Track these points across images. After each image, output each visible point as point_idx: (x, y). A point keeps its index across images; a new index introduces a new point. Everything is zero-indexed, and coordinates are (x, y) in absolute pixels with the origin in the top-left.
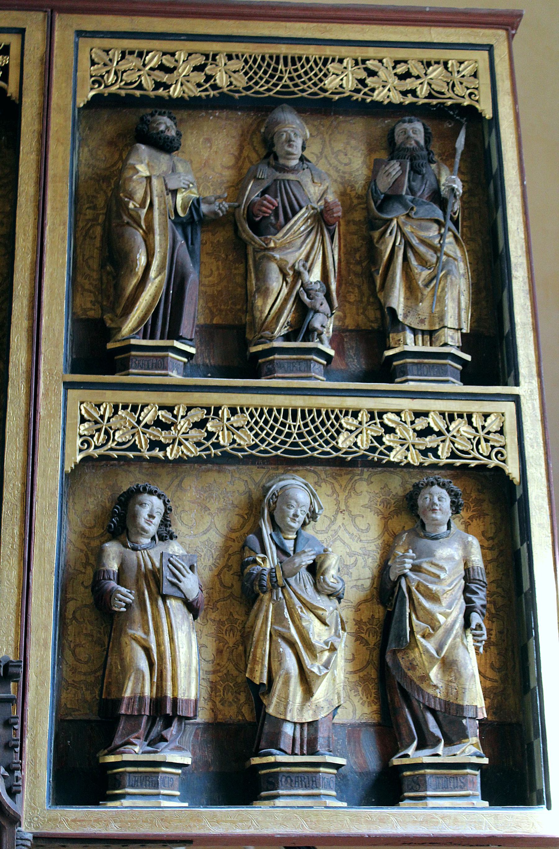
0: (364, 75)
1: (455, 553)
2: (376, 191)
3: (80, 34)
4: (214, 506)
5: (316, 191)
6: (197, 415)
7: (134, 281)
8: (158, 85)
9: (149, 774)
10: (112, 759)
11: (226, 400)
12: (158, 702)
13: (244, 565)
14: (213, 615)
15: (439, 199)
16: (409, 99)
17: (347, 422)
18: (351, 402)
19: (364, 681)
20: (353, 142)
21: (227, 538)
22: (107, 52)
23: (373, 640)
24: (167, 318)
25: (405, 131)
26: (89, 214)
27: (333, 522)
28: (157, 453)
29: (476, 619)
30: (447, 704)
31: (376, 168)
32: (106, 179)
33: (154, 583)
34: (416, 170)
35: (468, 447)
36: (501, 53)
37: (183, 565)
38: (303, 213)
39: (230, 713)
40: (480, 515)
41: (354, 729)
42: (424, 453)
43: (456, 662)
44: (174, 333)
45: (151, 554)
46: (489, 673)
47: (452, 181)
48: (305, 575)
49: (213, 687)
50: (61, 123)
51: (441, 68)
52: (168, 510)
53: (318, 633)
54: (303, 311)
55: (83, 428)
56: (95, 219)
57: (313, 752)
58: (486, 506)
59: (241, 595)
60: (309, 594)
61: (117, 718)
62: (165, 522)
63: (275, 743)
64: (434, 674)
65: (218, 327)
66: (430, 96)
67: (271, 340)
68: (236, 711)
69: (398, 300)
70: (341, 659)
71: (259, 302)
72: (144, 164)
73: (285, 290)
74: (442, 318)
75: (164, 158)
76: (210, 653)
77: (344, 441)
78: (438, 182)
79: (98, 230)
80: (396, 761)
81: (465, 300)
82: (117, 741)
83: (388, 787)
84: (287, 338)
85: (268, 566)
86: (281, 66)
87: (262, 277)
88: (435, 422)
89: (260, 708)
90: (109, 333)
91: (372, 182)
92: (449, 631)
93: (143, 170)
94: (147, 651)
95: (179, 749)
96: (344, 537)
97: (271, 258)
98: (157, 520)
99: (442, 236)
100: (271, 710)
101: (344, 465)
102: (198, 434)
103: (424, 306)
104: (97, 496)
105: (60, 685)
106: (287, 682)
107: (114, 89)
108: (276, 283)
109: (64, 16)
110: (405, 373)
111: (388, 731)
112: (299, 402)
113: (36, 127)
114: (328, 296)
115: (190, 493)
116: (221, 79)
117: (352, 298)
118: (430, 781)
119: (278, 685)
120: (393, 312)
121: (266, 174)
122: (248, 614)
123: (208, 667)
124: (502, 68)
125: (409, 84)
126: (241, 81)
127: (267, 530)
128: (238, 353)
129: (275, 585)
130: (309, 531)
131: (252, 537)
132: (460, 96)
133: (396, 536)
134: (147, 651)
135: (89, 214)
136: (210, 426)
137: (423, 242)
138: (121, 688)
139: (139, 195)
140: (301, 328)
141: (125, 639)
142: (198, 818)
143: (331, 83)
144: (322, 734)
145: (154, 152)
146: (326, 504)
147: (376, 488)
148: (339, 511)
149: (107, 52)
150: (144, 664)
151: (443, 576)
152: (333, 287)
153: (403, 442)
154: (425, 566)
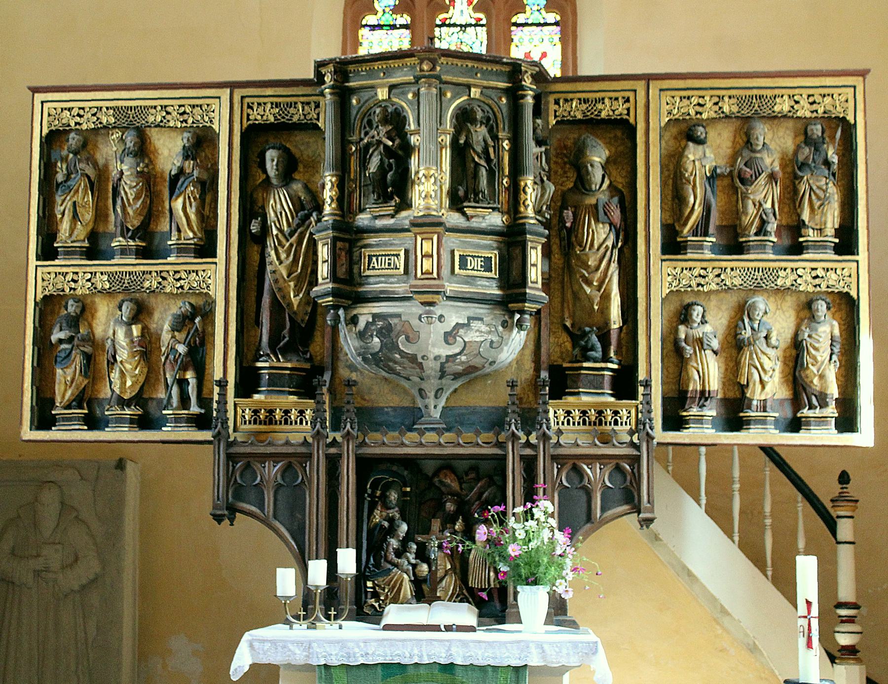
0: (793, 103)
1: (827, 329)
2: (797, 161)
3: (661, 90)
4: (724, 307)
5: (770, 161)
6: (717, 272)
7: (689, 210)
8: (697, 113)
9: (700, 420)
10: (685, 414)
11: (729, 265)
12: (703, 392)
13: (736, 335)
14: (724, 354)
15: (827, 163)
16: (815, 115)
17: (782, 273)
18: (783, 265)
19: (787, 381)
20: (788, 132)
21: (729, 322)
22: (673, 97)
23: (791, 364)
24: (702, 229)
25: (812, 130)
26: (667, 173)
27: (775, 314)
28: (700, 288)
29: (835, 357)
30: (821, 393)
31: (798, 148)
32: (673, 156)
33: (700, 343)
34: (816, 150)
35: (834, 283)
36: (860, 89)
37: (711, 336)
38: (764, 175)
39: (731, 395)
40: (840, 310)
41: (782, 401)
42: (182, 122)
43: (825, 374)
44: (706, 234)
45: (698, 331)
46: (841, 378)
47: (833, 156)
48: (763, 340)
49: (724, 384)
50: (654, 136)
51: (830, 98)
52: (704, 311)
53: (768, 364)
54: (763, 223)
55: (669, 279)
56: (669, 176)
57: (765, 411)
58: (843, 306)
59: (735, 346)
60: (764, 347)
61: (686, 398)
62: (703, 316)
63: (749, 408)
64: (816, 381)
65: (725, 226)
66: (825, 112)
67: (749, 236)
68: (733, 394)
69: (806, 216)
70: (777, 376)
71: (743, 218)
72: (692, 153)
73: (755, 212)
74: (825, 224)
75: (700, 147)
76: (723, 370)
77: (779, 282)
78: (827, 155)
79: (671, 181)
80: (799, 415)
81: (837, 213)
82: (687, 407)
83: (795, 425)
84: (756, 234)
85: (747, 336)
86: (754, 100)
87: (745, 206)
88: (820, 272)
89: (743, 393)
90: (677, 233)
91: (796, 153)
92: (823, 363)
93: (691, 157)
94: (698, 372)
95: (710, 409)
96: (777, 321)
97: (749, 198)
98: (700, 316)
99: (827, 184)
100: (748, 395)
101: (781, 292)
102: (717, 280)
103: (817, 217)
104: (674, 306)
105: (663, 383)
106: (754, 385)
107: (677, 117)
108: (751, 210)
109: (655, 82)
110: (807, 249)
111: (796, 402)
112: (761, 265)
113: (644, 139)
114: (774, 214)
115: (714, 301)
116: (726, 109)
117: (786, 210)
118: (813, 423)
119: (751, 385)
120: (803, 221)
121: (746, 154)
122: (738, 353)
123: (722, 376)
124: (860, 98)
125: (814, 107)
126: (735, 109)
127: (746, 320)
128: (734, 244)
129: (750, 344)
130: (764, 319)
131: (740, 323)
132: (839, 112)
133: (802, 320)
134: (698, 372)
135: (667, 173)
136: (722, 277)
137: (818, 188)
138: (688, 386)
139: (690, 170)
140: (762, 230)
141: (689, 367)
142: (719, 437)
143: (777, 108)
144: (768, 404)
145: (696, 146)
146: (772, 307)
147: (794, 298)
148: (777, 309)
149: (673, 97)
150: (697, 377)
151: (821, 340)
152: (777, 209)
153: (806, 282)
154: (814, 336)
